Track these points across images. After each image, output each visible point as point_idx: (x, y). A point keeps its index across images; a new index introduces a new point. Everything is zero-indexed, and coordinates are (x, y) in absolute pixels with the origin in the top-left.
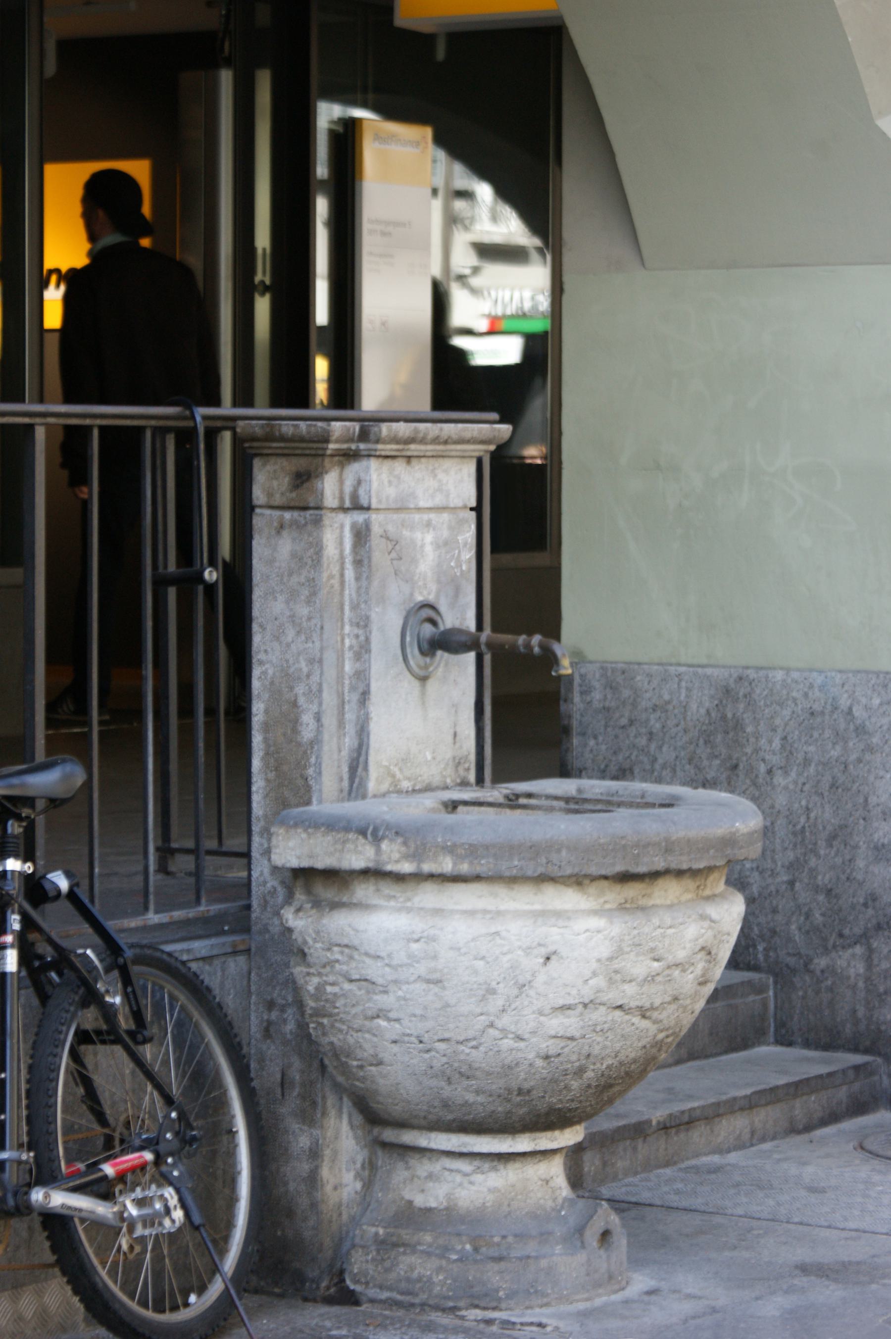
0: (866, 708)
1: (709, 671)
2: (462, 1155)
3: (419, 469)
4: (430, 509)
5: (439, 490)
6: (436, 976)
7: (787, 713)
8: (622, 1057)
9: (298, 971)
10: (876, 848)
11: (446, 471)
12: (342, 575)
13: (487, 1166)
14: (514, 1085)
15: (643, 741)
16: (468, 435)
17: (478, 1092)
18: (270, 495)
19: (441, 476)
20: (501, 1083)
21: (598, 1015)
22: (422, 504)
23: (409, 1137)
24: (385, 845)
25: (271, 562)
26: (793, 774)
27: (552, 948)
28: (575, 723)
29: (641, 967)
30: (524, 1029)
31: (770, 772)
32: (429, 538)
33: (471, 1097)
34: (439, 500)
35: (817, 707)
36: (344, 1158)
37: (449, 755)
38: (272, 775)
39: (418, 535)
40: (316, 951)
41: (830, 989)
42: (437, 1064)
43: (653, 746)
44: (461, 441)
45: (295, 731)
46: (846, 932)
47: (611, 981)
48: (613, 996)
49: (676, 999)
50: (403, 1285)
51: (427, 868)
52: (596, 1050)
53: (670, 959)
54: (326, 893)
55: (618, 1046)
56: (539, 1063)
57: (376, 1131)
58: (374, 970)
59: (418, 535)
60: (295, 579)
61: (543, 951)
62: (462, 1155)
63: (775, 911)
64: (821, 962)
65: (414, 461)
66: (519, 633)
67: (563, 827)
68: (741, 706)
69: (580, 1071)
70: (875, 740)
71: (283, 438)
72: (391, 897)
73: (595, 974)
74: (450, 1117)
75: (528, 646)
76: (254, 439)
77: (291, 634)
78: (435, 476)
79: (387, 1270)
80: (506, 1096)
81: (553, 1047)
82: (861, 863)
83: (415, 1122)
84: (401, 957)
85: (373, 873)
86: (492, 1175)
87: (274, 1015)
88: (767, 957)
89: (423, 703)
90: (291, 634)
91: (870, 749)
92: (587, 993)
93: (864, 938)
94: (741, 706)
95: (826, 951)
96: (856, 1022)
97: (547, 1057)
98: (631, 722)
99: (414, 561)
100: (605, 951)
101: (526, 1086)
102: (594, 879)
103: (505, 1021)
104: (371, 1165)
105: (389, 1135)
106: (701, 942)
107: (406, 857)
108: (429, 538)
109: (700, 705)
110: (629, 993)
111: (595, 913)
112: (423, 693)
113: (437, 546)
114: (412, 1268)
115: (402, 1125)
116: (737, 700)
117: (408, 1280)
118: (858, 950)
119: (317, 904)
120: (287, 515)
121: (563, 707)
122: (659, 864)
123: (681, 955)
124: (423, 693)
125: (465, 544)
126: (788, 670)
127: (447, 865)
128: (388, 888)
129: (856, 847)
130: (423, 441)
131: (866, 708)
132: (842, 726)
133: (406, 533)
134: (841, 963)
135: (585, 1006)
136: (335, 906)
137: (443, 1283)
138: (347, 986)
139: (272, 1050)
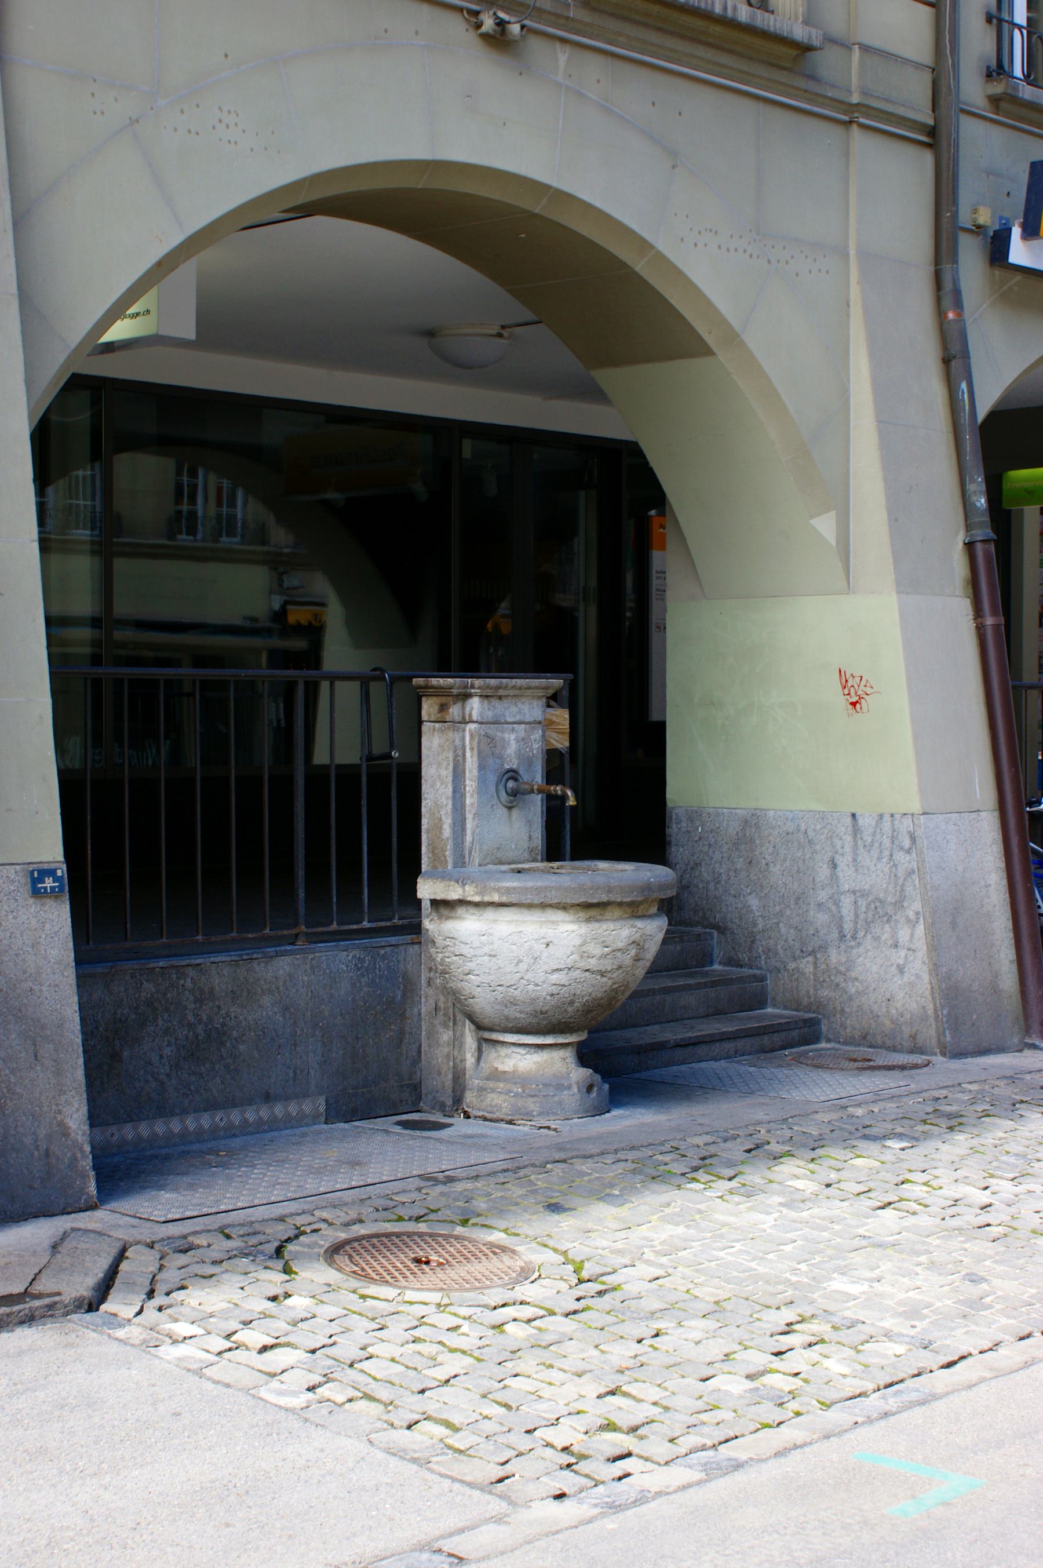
0: (814, 830)
1: (738, 811)
2: (520, 1045)
3: (506, 703)
4: (514, 723)
5: (520, 712)
6: (493, 953)
7: (775, 833)
8: (594, 995)
9: (432, 950)
10: (819, 905)
11: (523, 703)
12: (464, 755)
13: (532, 1051)
14: (538, 1009)
15: (706, 848)
16: (533, 685)
17: (521, 1012)
18: (429, 715)
20: (532, 1008)
21: (577, 974)
22: (509, 720)
23: (495, 1036)
24: (467, 888)
25: (429, 749)
26: (779, 866)
27: (549, 940)
28: (673, 839)
29: (598, 951)
30: (539, 981)
31: (767, 864)
32: (513, 736)
33: (518, 1015)
34: (518, 718)
35: (790, 830)
36: (467, 1046)
37: (526, 847)
38: (430, 855)
39: (506, 735)
40: (439, 941)
41: (797, 980)
42: (499, 998)
43: (711, 851)
44: (529, 688)
45: (440, 833)
46: (804, 949)
47: (582, 957)
48: (582, 964)
49: (620, 967)
50: (489, 1109)
51: (486, 899)
52: (578, 992)
53: (615, 947)
54: (444, 911)
55: (590, 990)
56: (549, 998)
57: (481, 1033)
58: (465, 950)
59: (506, 735)
60: (440, 757)
61: (545, 941)
62: (520, 1045)
63: (770, 938)
64: (792, 965)
66: (552, 784)
68: (753, 830)
69: (572, 1003)
70: (818, 847)
71: (432, 687)
72: (473, 914)
73: (572, 953)
74: (511, 1025)
75: (555, 791)
76: (421, 687)
77: (438, 784)
79: (482, 1101)
80: (535, 1014)
81: (555, 990)
82: (812, 913)
83: (496, 1028)
84: (476, 944)
85: (462, 902)
86: (535, 1055)
87: (432, 974)
88: (766, 962)
90: (438, 784)
91: (815, 852)
92: (570, 962)
93: (813, 953)
94: (753, 830)
95: (795, 959)
96: (810, 998)
97: (552, 995)
98: (700, 839)
99: (504, 748)
100: (578, 942)
101: (544, 1009)
102: (551, 906)
103: (528, 976)
104: (480, 1050)
105: (487, 1035)
106: (632, 939)
107: (477, 894)
108: (513, 736)
109: (733, 829)
110: (592, 963)
111: (573, 922)
112: (510, 816)
113: (517, 741)
114: (493, 1100)
115: (491, 1030)
116: (751, 827)
117: (491, 1106)
118: (810, 959)
119: (440, 917)
120: (437, 725)
121: (667, 831)
122: (604, 898)
123: (620, 945)
124: (510, 816)
126: (775, 810)
127: (496, 898)
128: (472, 910)
129: (809, 904)
130: (506, 687)
131: (814, 830)
132: (802, 840)
134: (802, 966)
135: (569, 969)
136: (448, 918)
137: (506, 1107)
138: (455, 958)
139: (431, 991)
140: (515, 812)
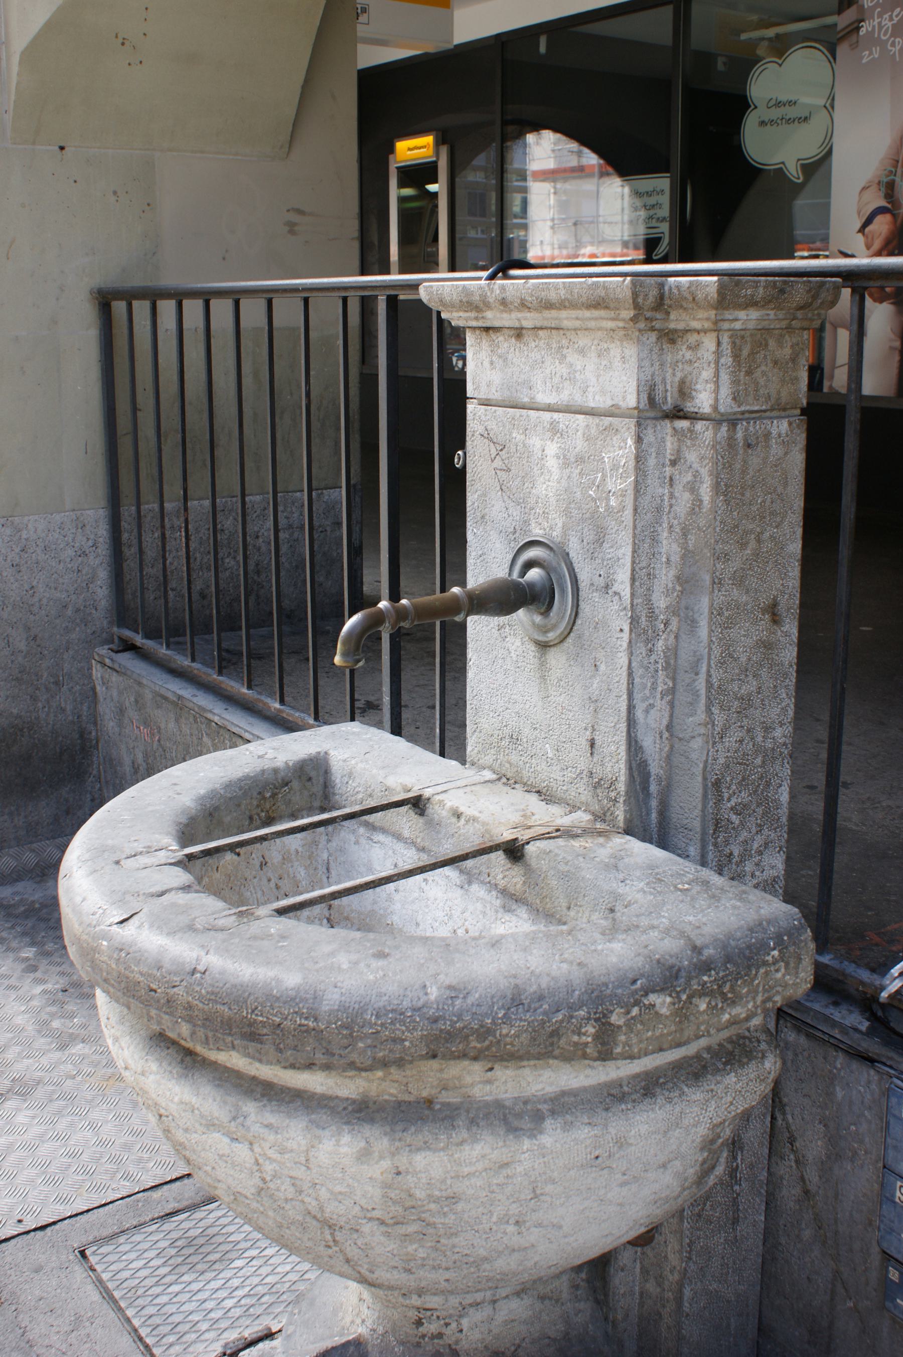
5: (571, 379)
11: (582, 352)
19: (572, 357)
22: (543, 398)
32: (552, 448)
34: (563, 397)
39: (535, 442)
65: (528, 337)
67: (111, 724)
78: (564, 357)
89: (543, 678)
108: (552, 448)
124: (542, 664)
125: (615, 467)
133: (517, 436)
140: (557, 659)
